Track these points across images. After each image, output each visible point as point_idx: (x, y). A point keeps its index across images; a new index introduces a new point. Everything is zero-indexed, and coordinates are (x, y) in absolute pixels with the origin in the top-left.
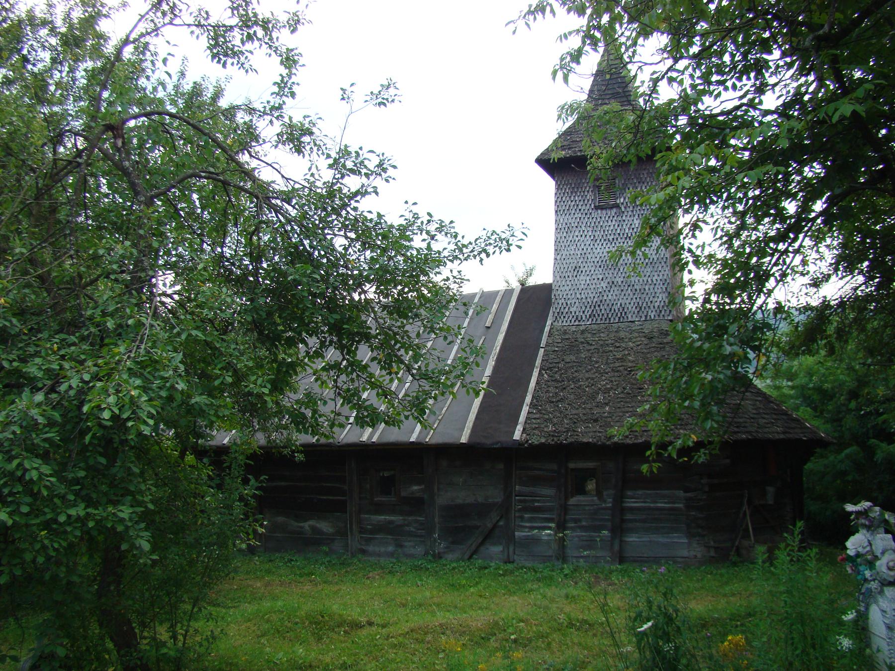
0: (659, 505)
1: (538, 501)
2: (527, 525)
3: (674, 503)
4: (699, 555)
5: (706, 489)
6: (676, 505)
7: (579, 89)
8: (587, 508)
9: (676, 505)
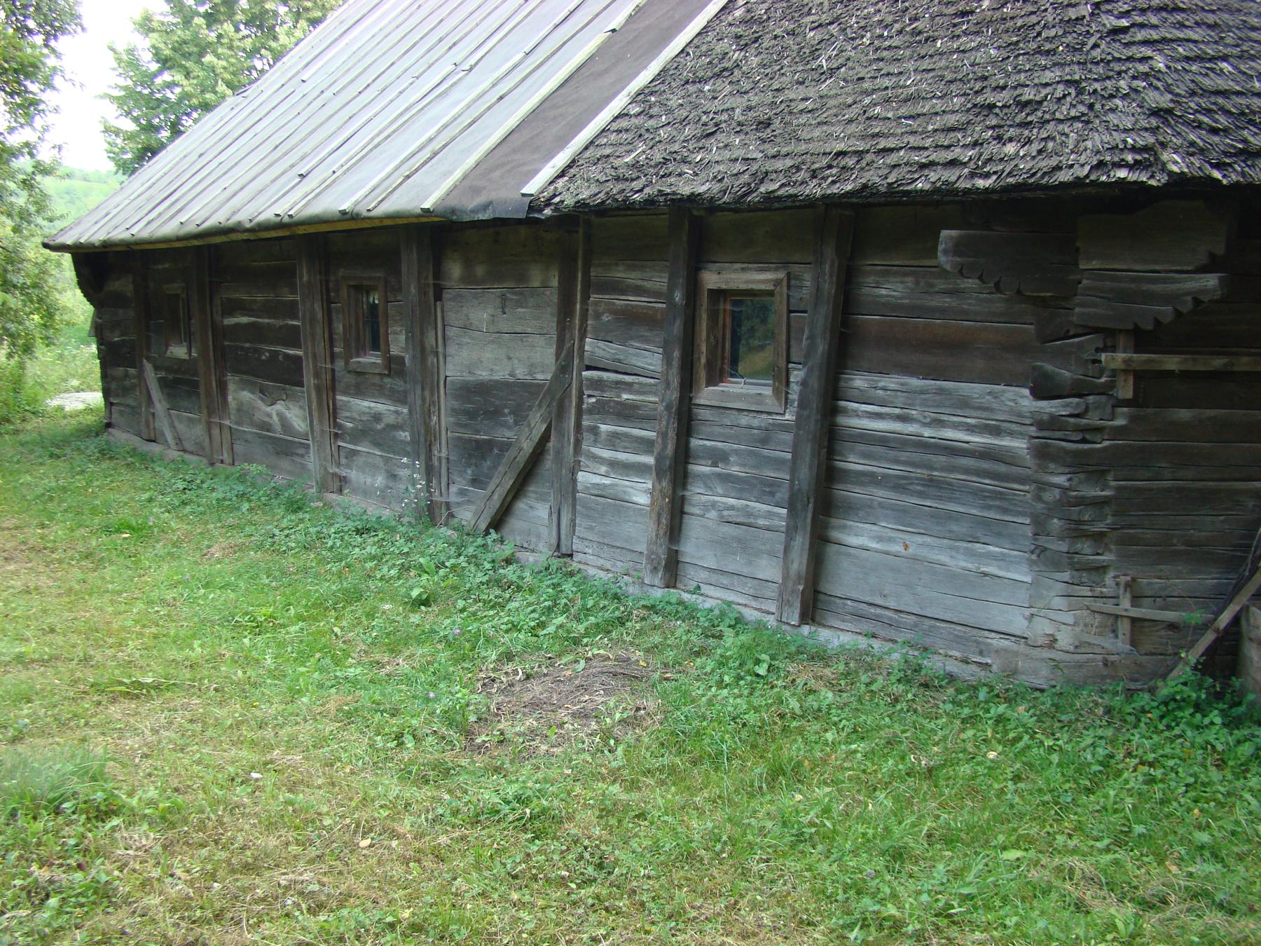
0: (950, 434)
1: (629, 387)
2: (606, 454)
3: (996, 431)
4: (1065, 639)
5: (1126, 390)
6: (1006, 442)
7: (298, 179)
8: (744, 420)
9: (1006, 442)
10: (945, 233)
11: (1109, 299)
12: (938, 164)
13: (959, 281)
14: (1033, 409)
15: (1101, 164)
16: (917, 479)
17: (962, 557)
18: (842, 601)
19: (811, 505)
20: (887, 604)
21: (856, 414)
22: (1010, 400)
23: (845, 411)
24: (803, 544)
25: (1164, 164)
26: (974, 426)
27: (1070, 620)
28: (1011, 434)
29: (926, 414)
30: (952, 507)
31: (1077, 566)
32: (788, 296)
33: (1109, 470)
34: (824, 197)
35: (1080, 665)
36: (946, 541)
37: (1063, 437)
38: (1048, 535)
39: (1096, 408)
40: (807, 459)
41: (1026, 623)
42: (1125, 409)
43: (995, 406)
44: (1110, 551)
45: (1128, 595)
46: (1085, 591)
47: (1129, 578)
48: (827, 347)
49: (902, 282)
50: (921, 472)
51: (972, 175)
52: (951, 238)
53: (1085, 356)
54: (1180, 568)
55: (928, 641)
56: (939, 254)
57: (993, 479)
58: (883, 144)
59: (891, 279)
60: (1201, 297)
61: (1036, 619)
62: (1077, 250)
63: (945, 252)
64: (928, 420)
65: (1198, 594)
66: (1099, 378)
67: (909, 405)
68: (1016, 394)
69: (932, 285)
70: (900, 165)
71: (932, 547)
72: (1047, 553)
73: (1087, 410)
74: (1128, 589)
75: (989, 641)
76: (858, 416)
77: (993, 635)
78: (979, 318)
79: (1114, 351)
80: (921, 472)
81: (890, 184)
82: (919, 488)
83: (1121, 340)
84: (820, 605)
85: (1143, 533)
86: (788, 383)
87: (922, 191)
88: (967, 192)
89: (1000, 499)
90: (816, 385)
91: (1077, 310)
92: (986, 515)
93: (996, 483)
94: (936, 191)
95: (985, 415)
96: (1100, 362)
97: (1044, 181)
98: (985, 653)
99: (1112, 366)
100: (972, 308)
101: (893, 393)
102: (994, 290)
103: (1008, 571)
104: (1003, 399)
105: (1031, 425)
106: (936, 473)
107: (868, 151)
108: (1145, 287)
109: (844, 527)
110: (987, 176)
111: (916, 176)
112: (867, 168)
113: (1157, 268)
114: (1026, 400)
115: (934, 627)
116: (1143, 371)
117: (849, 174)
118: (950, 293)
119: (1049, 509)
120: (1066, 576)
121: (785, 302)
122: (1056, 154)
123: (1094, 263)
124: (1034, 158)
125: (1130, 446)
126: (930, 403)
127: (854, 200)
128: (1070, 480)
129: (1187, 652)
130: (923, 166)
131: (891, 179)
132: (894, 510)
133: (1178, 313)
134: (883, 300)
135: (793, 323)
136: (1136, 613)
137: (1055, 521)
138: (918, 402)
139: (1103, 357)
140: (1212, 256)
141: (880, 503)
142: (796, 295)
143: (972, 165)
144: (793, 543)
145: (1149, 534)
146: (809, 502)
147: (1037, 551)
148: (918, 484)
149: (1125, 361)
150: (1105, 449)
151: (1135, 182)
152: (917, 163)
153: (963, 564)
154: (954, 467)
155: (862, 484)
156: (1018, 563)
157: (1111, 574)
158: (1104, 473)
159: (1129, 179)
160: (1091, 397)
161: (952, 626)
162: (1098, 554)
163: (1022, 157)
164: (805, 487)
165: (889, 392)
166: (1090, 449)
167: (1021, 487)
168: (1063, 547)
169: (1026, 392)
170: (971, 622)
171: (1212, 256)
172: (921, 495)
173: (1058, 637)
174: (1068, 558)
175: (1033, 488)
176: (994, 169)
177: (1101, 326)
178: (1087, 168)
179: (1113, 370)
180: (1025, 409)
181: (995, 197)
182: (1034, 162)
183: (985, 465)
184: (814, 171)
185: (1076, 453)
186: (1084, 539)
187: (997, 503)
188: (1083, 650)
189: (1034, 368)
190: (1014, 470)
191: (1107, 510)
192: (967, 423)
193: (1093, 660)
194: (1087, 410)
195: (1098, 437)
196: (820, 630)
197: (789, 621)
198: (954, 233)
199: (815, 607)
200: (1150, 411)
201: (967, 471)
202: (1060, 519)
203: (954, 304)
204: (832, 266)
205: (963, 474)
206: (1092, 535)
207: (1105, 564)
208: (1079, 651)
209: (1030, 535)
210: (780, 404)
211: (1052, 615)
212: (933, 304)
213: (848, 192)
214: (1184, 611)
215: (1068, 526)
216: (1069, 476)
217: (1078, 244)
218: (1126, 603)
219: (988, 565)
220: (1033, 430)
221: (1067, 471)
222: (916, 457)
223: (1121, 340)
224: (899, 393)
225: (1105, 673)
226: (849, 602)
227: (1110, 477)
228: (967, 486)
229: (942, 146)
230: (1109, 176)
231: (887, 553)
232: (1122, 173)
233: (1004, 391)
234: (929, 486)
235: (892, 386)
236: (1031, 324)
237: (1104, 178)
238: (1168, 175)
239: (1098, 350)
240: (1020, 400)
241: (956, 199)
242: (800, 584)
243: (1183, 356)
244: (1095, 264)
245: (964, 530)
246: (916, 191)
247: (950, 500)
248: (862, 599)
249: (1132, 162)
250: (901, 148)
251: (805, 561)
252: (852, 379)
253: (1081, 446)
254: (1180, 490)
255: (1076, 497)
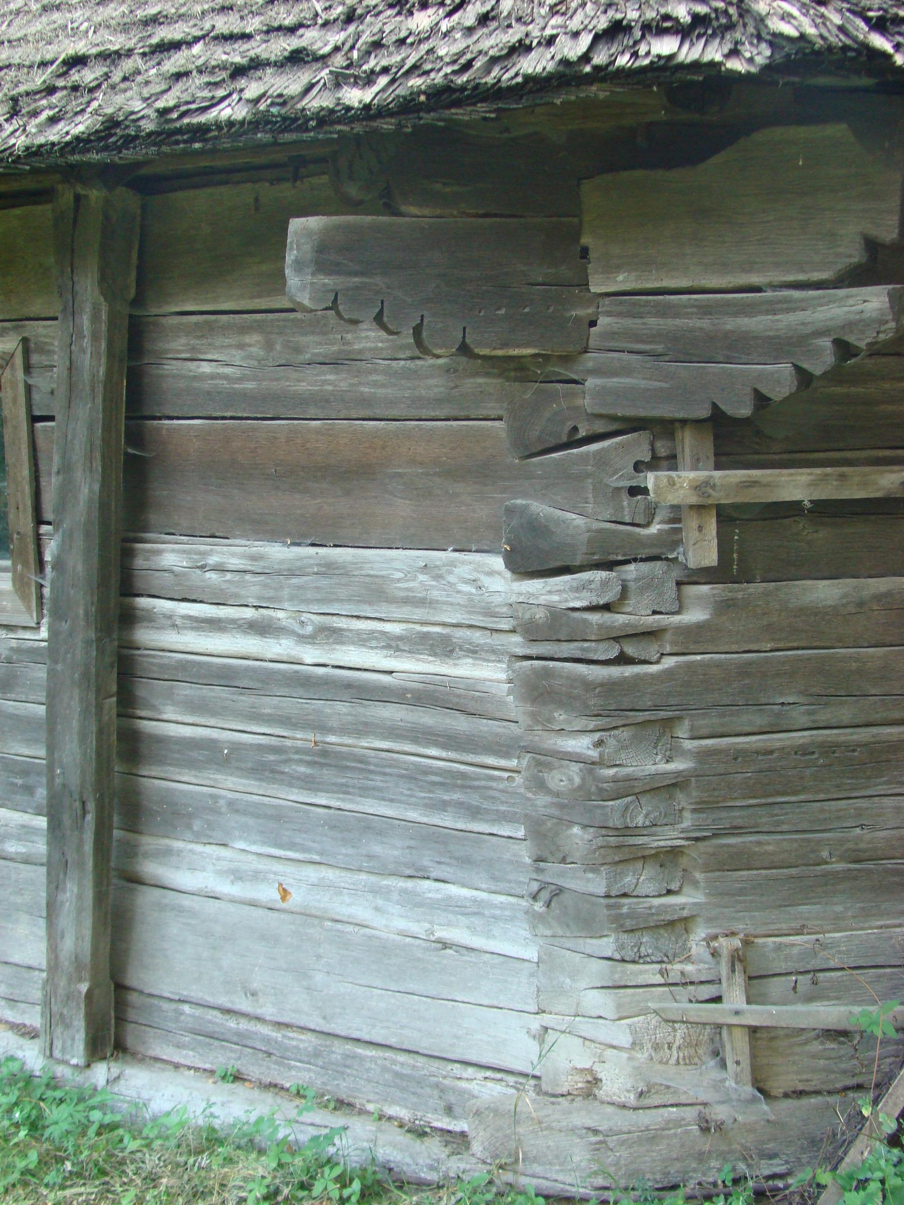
0: (352, 655)
10: (296, 224)
11: (657, 355)
12: (268, 64)
13: (349, 336)
14: (514, 599)
15: (617, 29)
16: (298, 751)
17: (397, 909)
18: (173, 1006)
19: (90, 818)
20: (259, 1011)
21: (172, 623)
22: (467, 582)
23: (150, 618)
24: (80, 897)
25: (761, 20)
26: (400, 638)
27: (625, 1039)
28: (474, 651)
29: (305, 617)
30: (370, 806)
31: (628, 924)
32: (29, 389)
33: (680, 718)
34: (33, 152)
35: (651, 1137)
36: (363, 876)
37: (578, 654)
38: (563, 860)
39: (642, 590)
40: (75, 723)
41: (533, 1047)
42: (705, 589)
43: (435, 594)
44: (695, 883)
45: (739, 978)
46: (649, 973)
47: (737, 942)
48: (97, 487)
49: (241, 346)
50: (302, 738)
51: (339, 80)
52: (308, 233)
53: (615, 481)
54: (839, 908)
55: (343, 1088)
56: (287, 271)
57: (444, 747)
58: (164, 33)
59: (219, 341)
60: (851, 339)
61: (551, 1037)
62: (584, 253)
63: (299, 265)
64: (309, 629)
65: (880, 961)
66: (648, 525)
67: (270, 599)
68: (478, 568)
69: (298, 350)
70: (187, 74)
71: (337, 890)
72: (566, 897)
73: (624, 593)
74: (738, 967)
75: (463, 1084)
76: (174, 626)
77: (470, 1072)
78: (395, 413)
79: (674, 468)
80: (302, 738)
81: (163, 112)
82: (302, 769)
83: (687, 441)
84: (132, 1015)
85: (759, 843)
86: (41, 564)
87: (231, 123)
88: (325, 118)
89: (463, 787)
90: (80, 568)
91: (591, 382)
92: (436, 820)
93: (451, 755)
94: (258, 122)
95: (419, 613)
96: (645, 491)
97: (490, 80)
98: (457, 1110)
99: (672, 498)
100: (381, 392)
101: (237, 577)
102: (417, 353)
103: (489, 935)
104: (451, 579)
105: (513, 631)
106: (332, 739)
107: (129, 53)
108: (730, 324)
109: (168, 852)
110: (369, 79)
111: (221, 93)
112: (123, 86)
113: (755, 279)
114: (497, 578)
115: (354, 1057)
116: (735, 506)
117: (86, 98)
118: (333, 363)
119: (562, 807)
120: (607, 945)
121: (22, 400)
122: (519, 19)
123: (620, 278)
124: (470, 30)
125: (718, 665)
126: (309, 595)
127: (94, 157)
128: (599, 743)
129: (876, 1102)
130: (238, 72)
131: (167, 101)
132: (258, 816)
133: (804, 377)
134: (207, 385)
135: (41, 442)
136: (756, 1015)
137: (576, 830)
138: (286, 592)
139: (651, 479)
140: (871, 245)
141: (231, 803)
142: (42, 382)
143: (339, 60)
144: (61, 897)
145: (770, 844)
146: (84, 812)
147: (545, 895)
148: (301, 761)
149: (699, 487)
150: (669, 673)
151: (696, 65)
152: (223, 67)
153: (401, 924)
154: (366, 724)
155: (193, 765)
156: (513, 919)
157: (700, 932)
158: (668, 724)
159: (681, 57)
160: (632, 567)
161: (389, 1054)
162: (669, 892)
163: (445, 35)
164: (74, 780)
165: (229, 576)
166: (637, 676)
167: (503, 763)
168: (596, 884)
169: (497, 562)
170: (424, 1045)
171: (871, 245)
172: (309, 784)
173: (600, 1076)
174: (608, 906)
175: (525, 762)
176: (385, 63)
177: (642, 413)
178: (586, 40)
179: (676, 508)
180: (497, 599)
181: (387, 125)
182: (470, 41)
183: (427, 718)
184: (15, 100)
185: (610, 687)
186: (639, 864)
187: (456, 796)
188: (656, 1100)
189: (510, 511)
190: (484, 726)
191: (682, 799)
192: (384, 633)
193: (679, 1123)
194: (624, 593)
195: (651, 650)
196: (129, 1071)
197: (67, 1057)
198: (314, 222)
199: (121, 1020)
200: (756, 588)
201: (393, 732)
202: (585, 827)
203: (344, 385)
204: (95, 318)
205: (384, 738)
206: (655, 856)
207: (685, 913)
208: (647, 1102)
209: (528, 860)
210: (29, 608)
211: (586, 1028)
212: (303, 387)
213: (77, 138)
214: (855, 1002)
215: (600, 841)
216: (597, 736)
217: (585, 240)
218: (735, 997)
219: (449, 924)
220: (516, 643)
221: (591, 726)
222: (292, 705)
223: (687, 441)
224: (248, 577)
225: (707, 1148)
226: (186, 1008)
227: (682, 731)
228: (394, 764)
229: (280, 28)
230: (635, 55)
231: (253, 904)
232: (665, 46)
233: (452, 564)
234: (322, 765)
235: (235, 563)
236: (500, 419)
237: (623, 60)
238: (771, 44)
239: (638, 467)
240: (486, 581)
241: (305, 136)
242: (80, 980)
243: (818, 471)
244: (623, 281)
245: (396, 853)
246: (218, 125)
247: (365, 792)
248: (210, 999)
249: (688, 19)
250: (197, 40)
251: (87, 932)
252: (159, 552)
253: (616, 672)
254: (828, 748)
255: (615, 780)
